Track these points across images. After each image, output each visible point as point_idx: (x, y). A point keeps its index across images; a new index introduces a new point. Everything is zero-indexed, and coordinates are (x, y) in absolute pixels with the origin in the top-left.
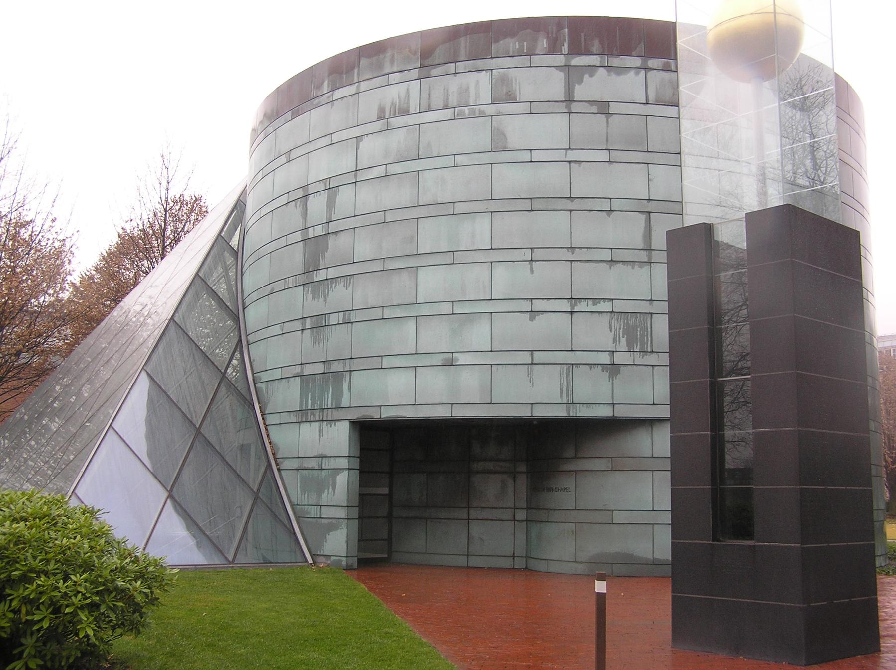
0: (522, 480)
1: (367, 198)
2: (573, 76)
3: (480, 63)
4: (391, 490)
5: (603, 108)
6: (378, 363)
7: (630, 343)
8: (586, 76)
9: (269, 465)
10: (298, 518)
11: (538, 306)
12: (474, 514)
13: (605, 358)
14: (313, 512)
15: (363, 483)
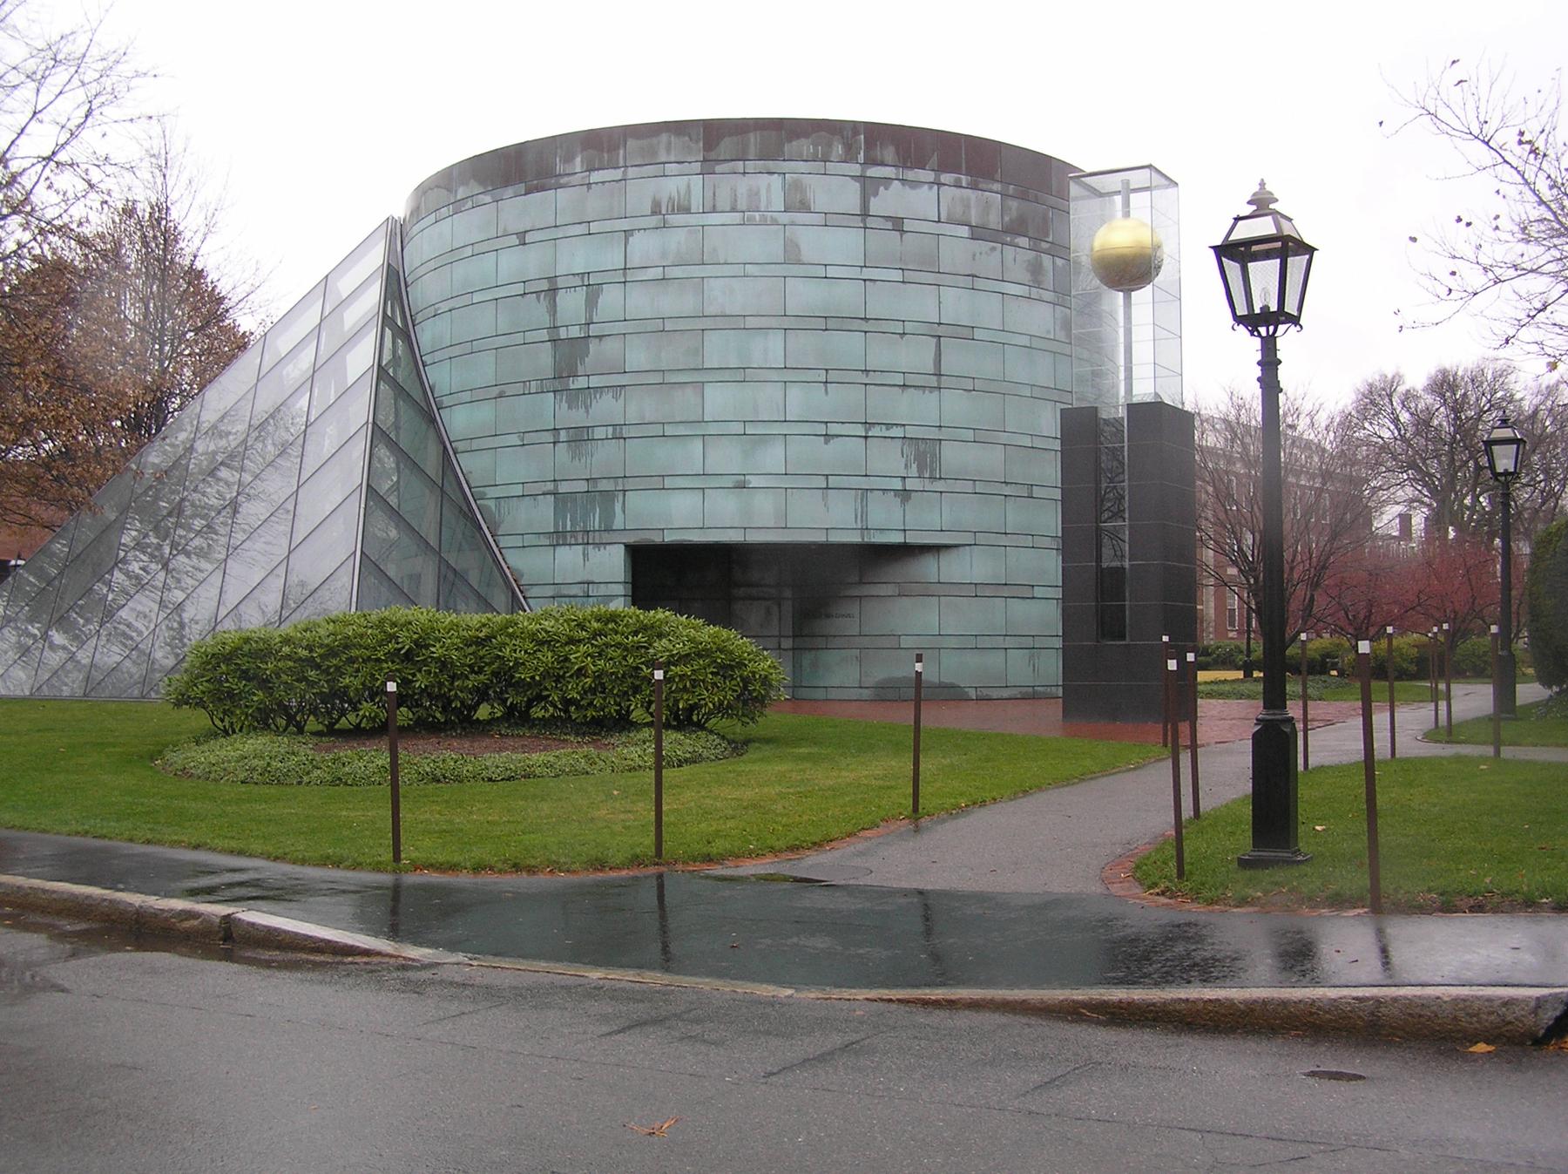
1: (641, 302)
2: (869, 187)
5: (897, 224)
6: (659, 483)
7: (920, 469)
9: (513, 592)
11: (834, 429)
13: (897, 484)
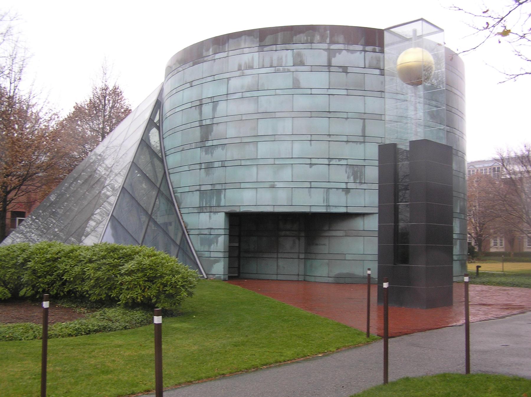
0: (303, 240)
2: (331, 53)
3: (288, 46)
4: (240, 245)
5: (344, 69)
6: (238, 186)
7: (355, 179)
8: (337, 54)
9: (184, 232)
10: (199, 257)
11: (314, 161)
12: (280, 255)
13: (343, 186)
14: (207, 254)
15: (230, 241)
